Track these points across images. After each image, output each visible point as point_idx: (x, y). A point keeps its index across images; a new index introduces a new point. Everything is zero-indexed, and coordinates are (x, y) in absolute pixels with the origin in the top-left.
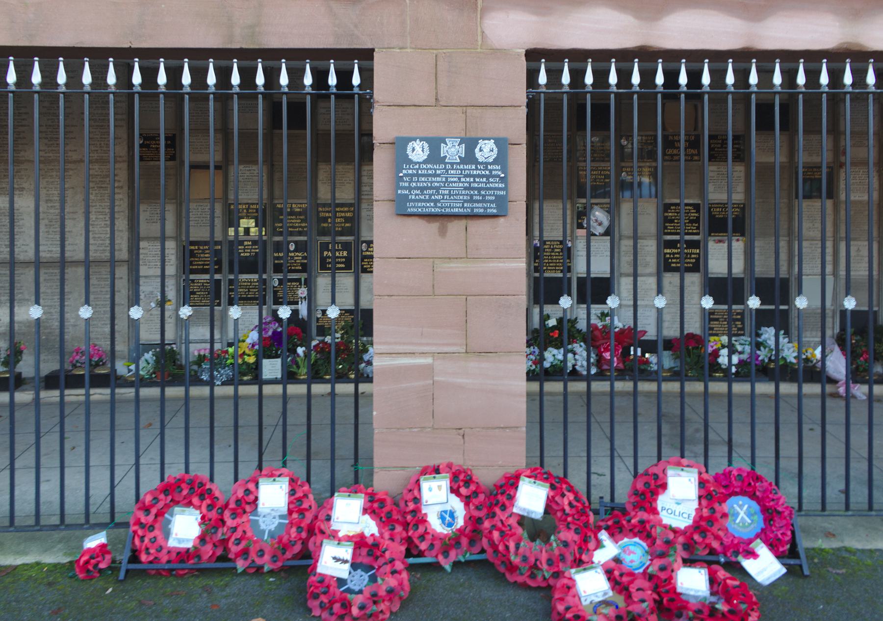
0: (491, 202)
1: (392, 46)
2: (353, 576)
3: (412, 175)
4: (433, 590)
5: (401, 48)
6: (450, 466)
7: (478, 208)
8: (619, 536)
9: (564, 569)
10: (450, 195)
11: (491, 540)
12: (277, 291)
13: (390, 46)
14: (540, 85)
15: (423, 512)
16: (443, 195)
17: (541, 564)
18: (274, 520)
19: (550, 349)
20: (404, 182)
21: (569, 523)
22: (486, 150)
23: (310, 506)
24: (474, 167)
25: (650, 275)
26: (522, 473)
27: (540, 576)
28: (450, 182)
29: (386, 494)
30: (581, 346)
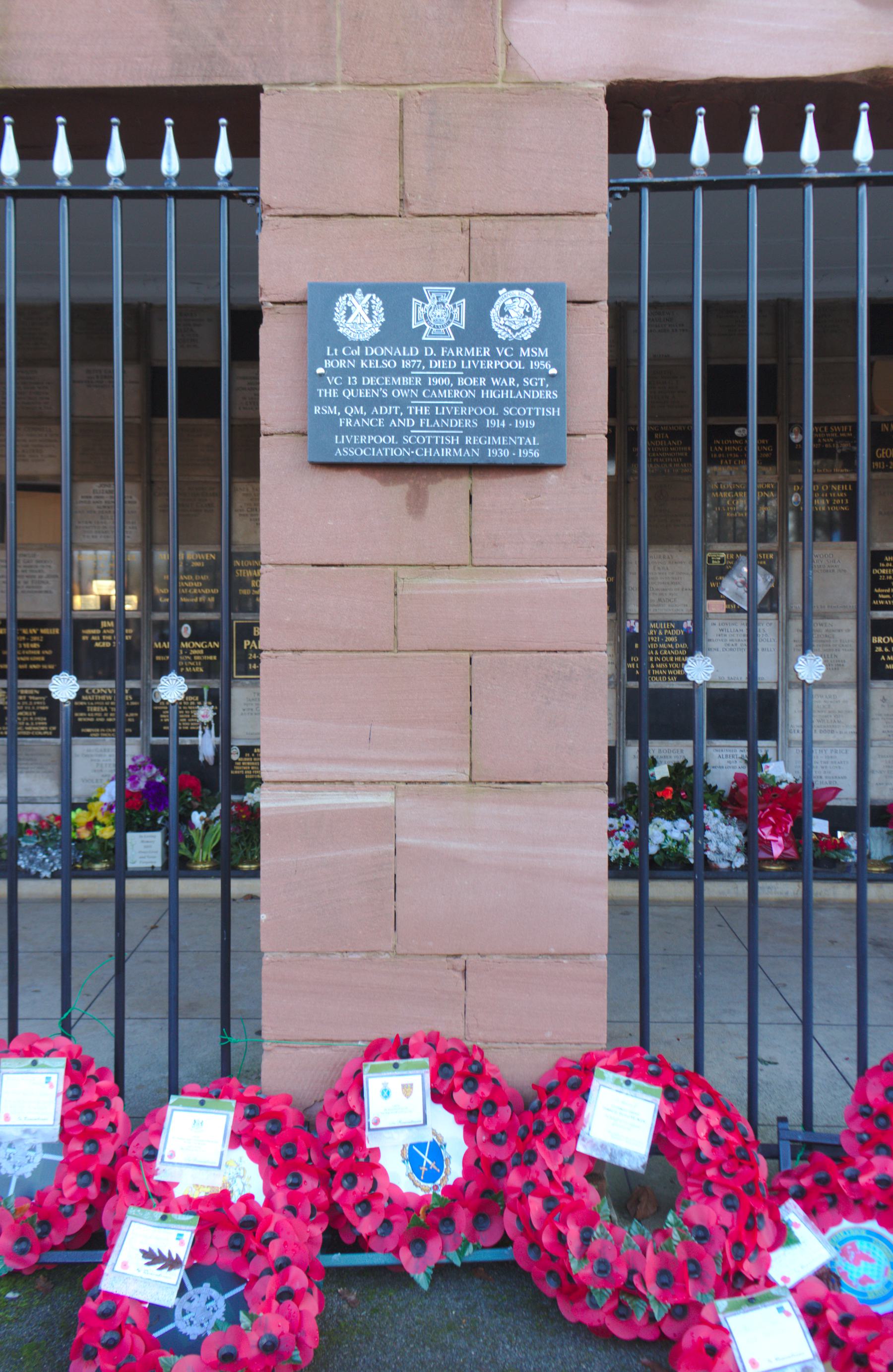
0: (526, 433)
1: (301, 78)
2: (190, 1300)
3: (344, 373)
4: (381, 1337)
5: (320, 84)
6: (433, 1039)
7: (496, 447)
8: (833, 1213)
9: (699, 1297)
10: (432, 417)
11: (524, 1217)
12: (161, 712)
13: (295, 79)
14: (640, 169)
15: (369, 1146)
16: (417, 418)
17: (644, 1283)
18: (32, 1154)
19: (658, 820)
20: (327, 386)
21: (710, 1181)
22: (516, 311)
23: (114, 1125)
24: (486, 352)
25: (845, 685)
26: (599, 1059)
27: (640, 1316)
28: (432, 388)
29: (288, 1100)
30: (715, 816)
